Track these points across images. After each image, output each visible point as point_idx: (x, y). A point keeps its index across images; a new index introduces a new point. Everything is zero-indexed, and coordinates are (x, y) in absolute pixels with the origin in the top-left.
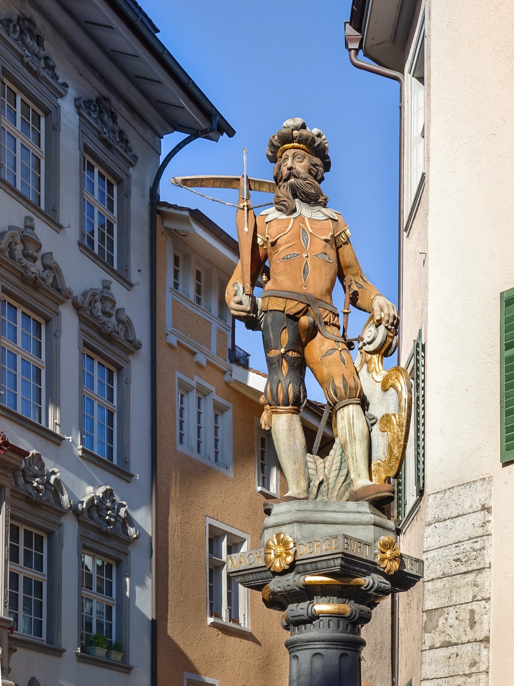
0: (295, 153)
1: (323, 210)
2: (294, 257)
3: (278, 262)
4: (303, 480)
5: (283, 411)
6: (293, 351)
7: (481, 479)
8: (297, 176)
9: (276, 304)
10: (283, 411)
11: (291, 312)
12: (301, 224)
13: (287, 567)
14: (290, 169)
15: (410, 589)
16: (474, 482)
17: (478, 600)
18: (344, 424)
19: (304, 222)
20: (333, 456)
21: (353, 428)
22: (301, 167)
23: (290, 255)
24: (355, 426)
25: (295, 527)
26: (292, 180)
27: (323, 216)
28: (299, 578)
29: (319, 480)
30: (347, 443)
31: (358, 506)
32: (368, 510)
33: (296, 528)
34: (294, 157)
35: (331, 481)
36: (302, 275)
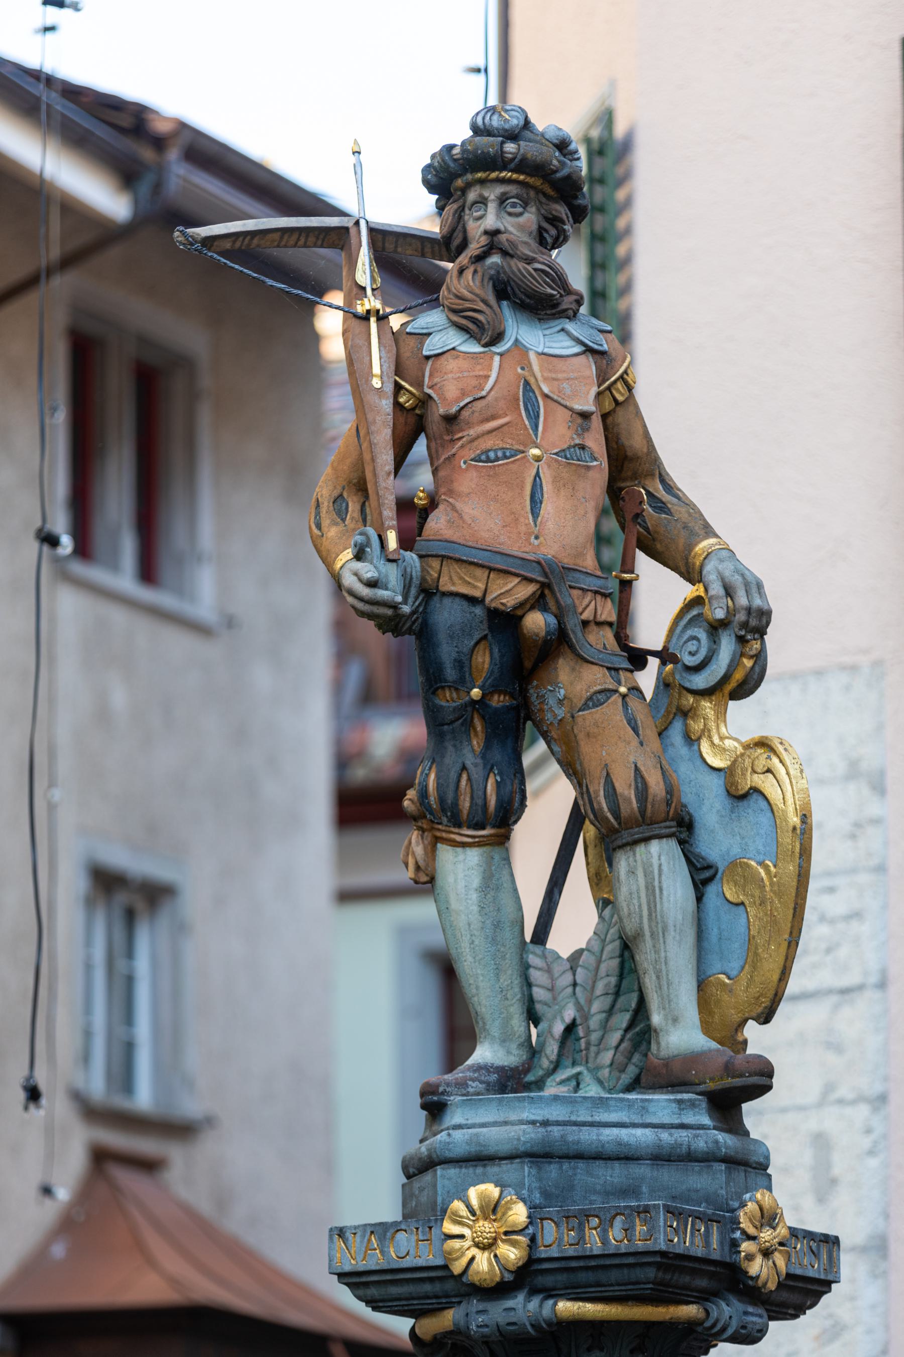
0: (503, 194)
1: (570, 326)
2: (506, 457)
3: (463, 466)
4: (517, 1016)
5: (470, 840)
6: (500, 693)
7: (843, 668)
8: (511, 252)
9: (461, 578)
10: (470, 840)
11: (502, 604)
12: (519, 370)
13: (508, 1277)
14: (493, 234)
15: (805, 1313)
16: (819, 673)
17: (841, 1102)
18: (634, 888)
19: (526, 365)
20: (598, 954)
21: (661, 898)
22: (521, 228)
23: (495, 451)
24: (665, 893)
25: (526, 1169)
26: (495, 259)
27: (570, 343)
28: (541, 1306)
29: (563, 1020)
30: (643, 935)
31: (680, 1109)
32: (706, 1120)
33: (529, 1173)
34: (502, 200)
35: (595, 1022)
36: (528, 508)
